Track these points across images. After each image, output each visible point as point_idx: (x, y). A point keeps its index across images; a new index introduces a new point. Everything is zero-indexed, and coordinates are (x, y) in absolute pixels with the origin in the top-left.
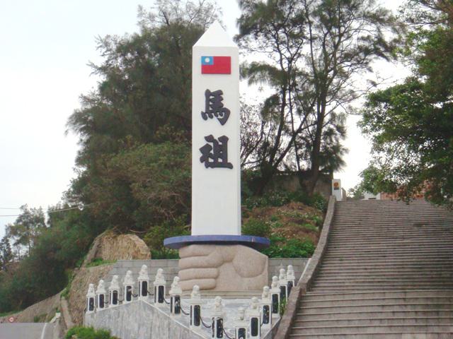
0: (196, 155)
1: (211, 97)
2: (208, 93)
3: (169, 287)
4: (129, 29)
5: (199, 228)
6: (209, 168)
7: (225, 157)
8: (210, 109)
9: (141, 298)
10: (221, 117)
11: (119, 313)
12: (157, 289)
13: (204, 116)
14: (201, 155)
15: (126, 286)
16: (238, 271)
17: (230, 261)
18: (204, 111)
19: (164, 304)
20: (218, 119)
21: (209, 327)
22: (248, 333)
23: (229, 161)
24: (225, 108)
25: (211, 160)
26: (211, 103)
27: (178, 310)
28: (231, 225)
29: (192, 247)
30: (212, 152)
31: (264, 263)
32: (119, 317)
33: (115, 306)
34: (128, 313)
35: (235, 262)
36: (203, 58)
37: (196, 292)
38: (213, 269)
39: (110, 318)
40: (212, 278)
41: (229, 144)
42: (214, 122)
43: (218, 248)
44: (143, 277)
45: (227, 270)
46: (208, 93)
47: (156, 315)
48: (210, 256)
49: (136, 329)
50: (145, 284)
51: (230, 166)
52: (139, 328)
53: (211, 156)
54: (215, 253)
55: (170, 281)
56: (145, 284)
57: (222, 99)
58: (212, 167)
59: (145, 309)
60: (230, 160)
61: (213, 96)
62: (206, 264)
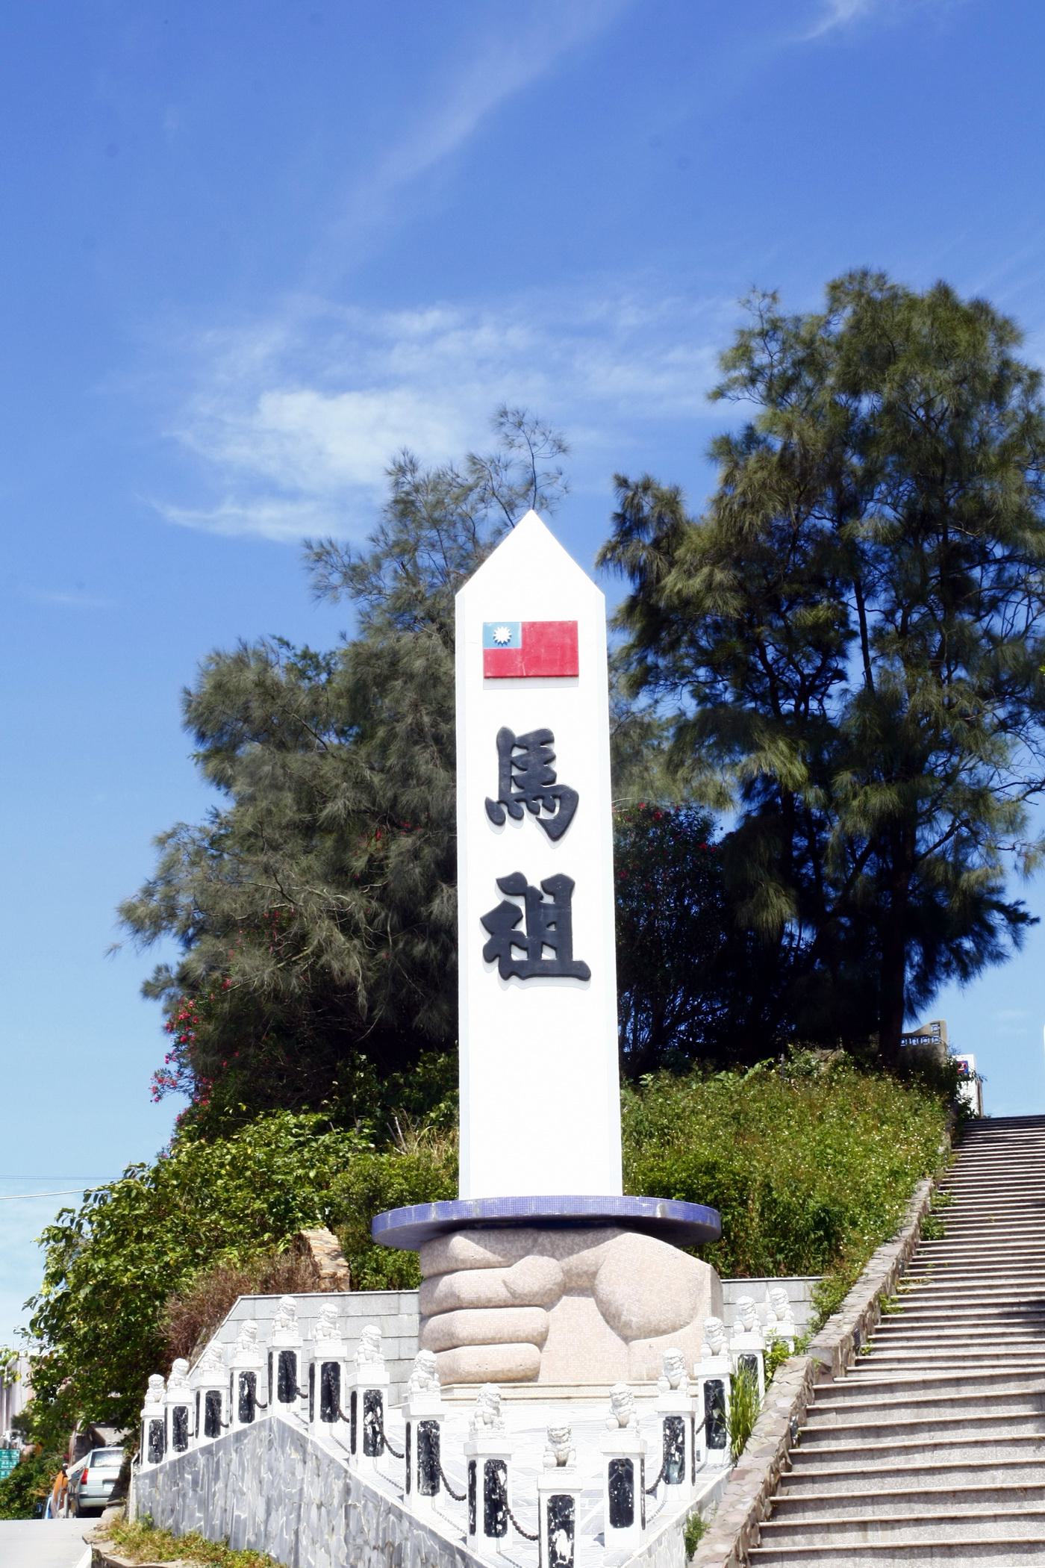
0: (472, 939)
2: (506, 741)
5: (487, 1177)
6: (514, 979)
7: (564, 944)
8: (514, 790)
9: (279, 1410)
11: (218, 1462)
13: (495, 814)
18: (495, 798)
19: (341, 1428)
20: (542, 822)
21: (464, 1498)
22: (592, 1509)
23: (576, 957)
24: (561, 787)
25: (518, 955)
26: (515, 772)
30: (522, 927)
32: (217, 1479)
34: (241, 1463)
36: (488, 630)
46: (506, 741)
51: (582, 973)
52: (268, 1513)
53: (518, 941)
57: (553, 758)
58: (523, 978)
59: (283, 1447)
60: (579, 953)
62: (503, 1294)
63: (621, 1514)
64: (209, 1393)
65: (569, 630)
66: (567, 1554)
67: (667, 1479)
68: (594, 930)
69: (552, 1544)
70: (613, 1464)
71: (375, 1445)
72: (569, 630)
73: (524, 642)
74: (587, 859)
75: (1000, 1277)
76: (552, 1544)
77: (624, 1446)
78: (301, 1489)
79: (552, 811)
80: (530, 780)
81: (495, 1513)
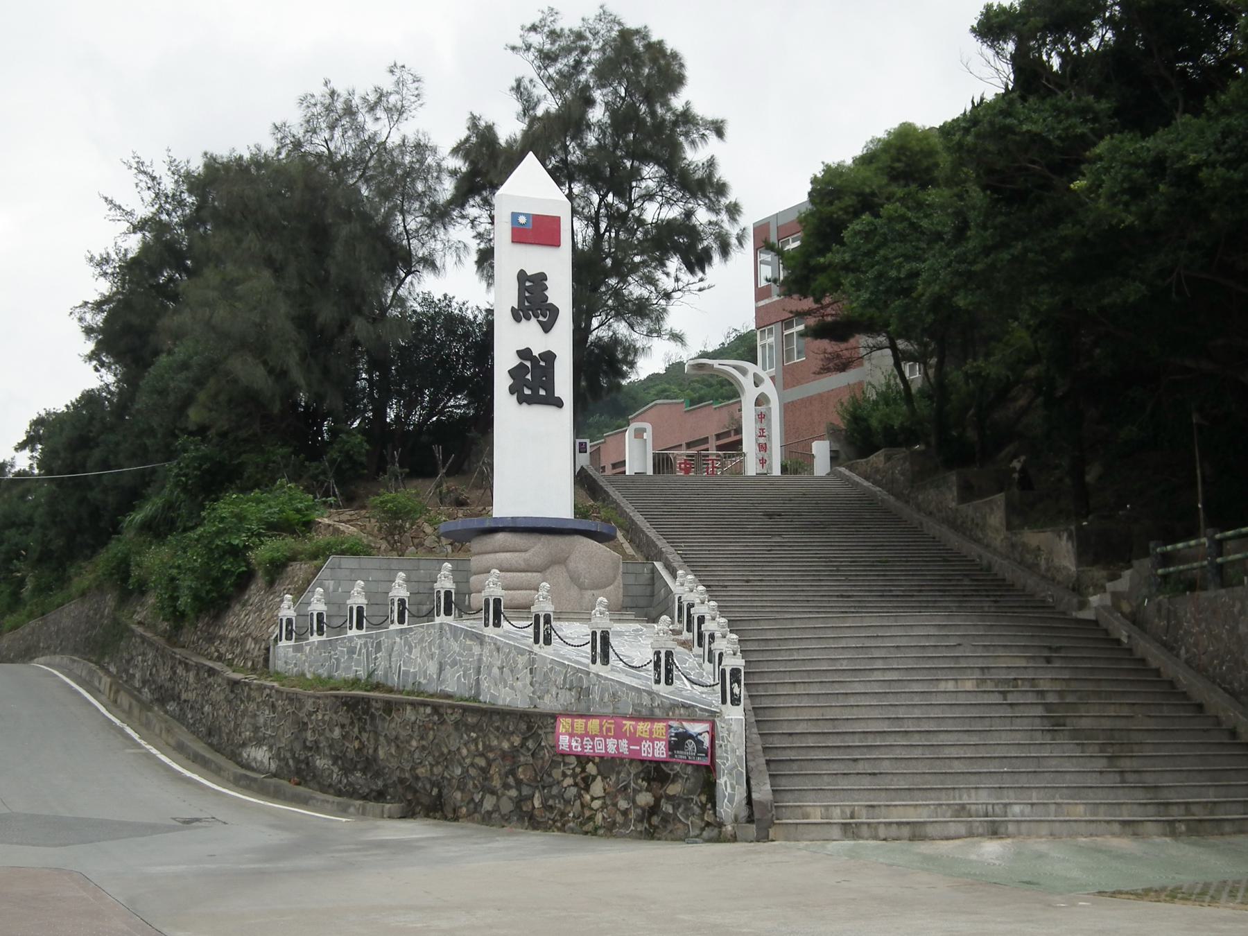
0: (502, 381)
1: (528, 284)
2: (522, 276)
4: (223, 152)
6: (525, 405)
7: (550, 385)
16: (575, 579)
25: (527, 392)
28: (559, 503)
29: (500, 537)
30: (529, 377)
35: (571, 565)
36: (515, 216)
39: (352, 651)
43: (545, 539)
46: (522, 276)
51: (559, 403)
54: (540, 548)
58: (529, 403)
62: (523, 565)
68: (564, 384)
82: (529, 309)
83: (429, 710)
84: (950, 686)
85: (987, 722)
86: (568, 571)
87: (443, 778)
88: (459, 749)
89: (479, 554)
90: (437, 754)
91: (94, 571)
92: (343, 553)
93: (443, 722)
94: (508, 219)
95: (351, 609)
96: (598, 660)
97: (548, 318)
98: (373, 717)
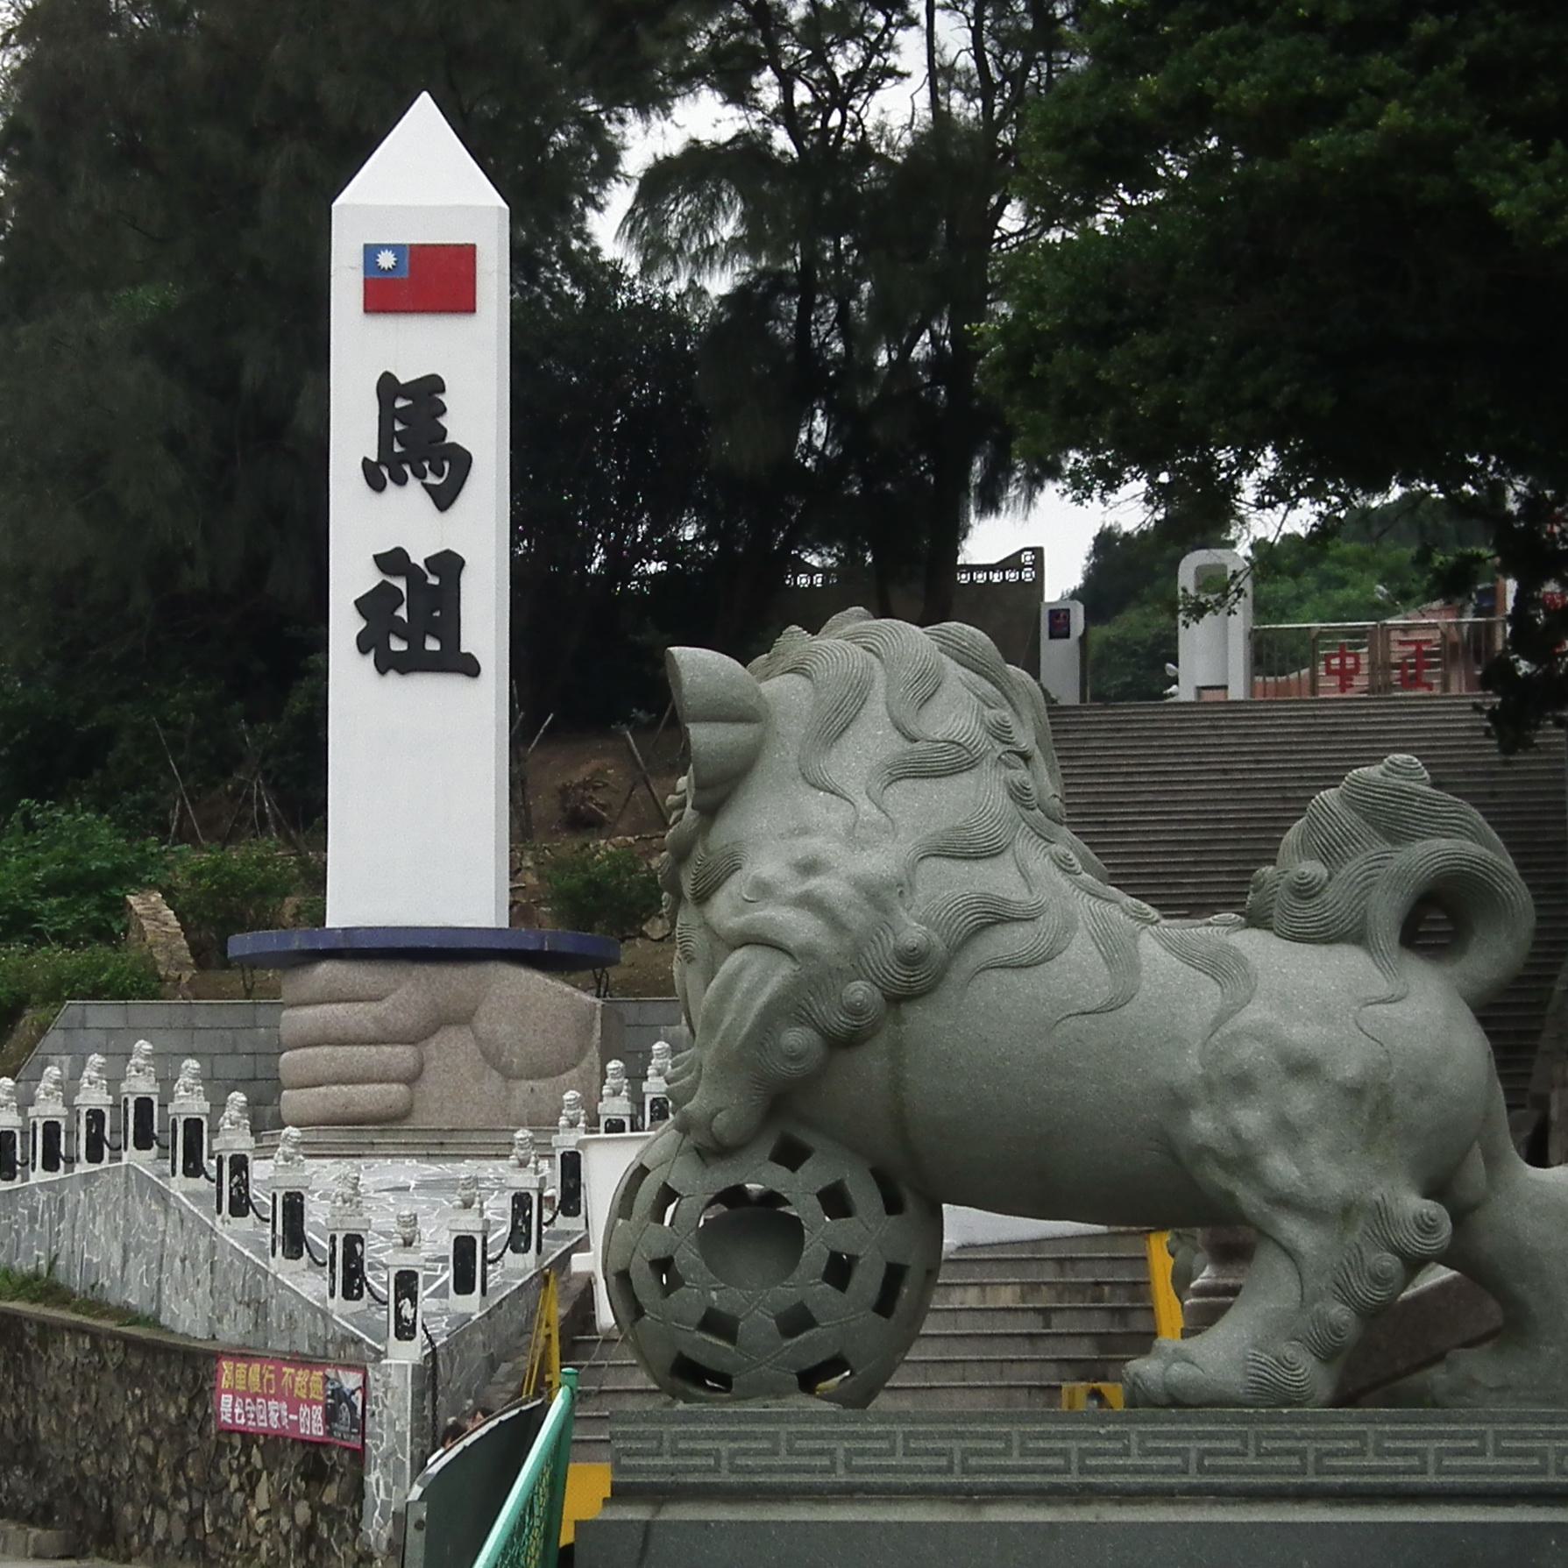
0: (344, 625)
1: (400, 403)
2: (388, 387)
3: (167, 1097)
6: (392, 675)
7: (450, 628)
8: (397, 449)
9: (131, 1155)
10: (438, 481)
11: (62, 1201)
12: (131, 1105)
14: (362, 624)
15: (84, 1111)
16: (492, 1057)
17: (462, 1018)
19: (201, 1184)
20: (425, 486)
23: (463, 650)
24: (454, 446)
25: (397, 645)
26: (398, 427)
27: (240, 1205)
29: (324, 969)
30: (402, 612)
31: (591, 1030)
32: (61, 1218)
33: (51, 1177)
34: (92, 1206)
35: (483, 1026)
36: (371, 252)
37: (235, 1114)
38: (399, 1049)
39: (33, 1218)
40: (397, 1081)
41: (467, 581)
42: (411, 498)
43: (430, 970)
44: (141, 1084)
45: (452, 1054)
46: (388, 387)
47: (175, 1217)
48: (386, 1004)
49: (116, 1261)
50: (144, 1105)
51: (470, 668)
54: (408, 993)
55: (167, 1083)
56: (144, 1105)
59: (142, 1197)
61: (405, 398)
62: (372, 1030)
63: (464, 1283)
64: (46, 1123)
65: (466, 254)
66: (410, 1317)
67: (515, 1250)
68: (485, 620)
69: (398, 1310)
70: (457, 1240)
71: (240, 1205)
72: (466, 254)
73: (412, 270)
74: (477, 531)
75: (1266, 810)
76: (398, 1310)
77: (469, 1223)
78: (163, 1241)
79: (440, 475)
80: (415, 435)
81: (353, 1282)
82: (402, 459)
83: (87, 1343)
84: (971, 1298)
85: (956, 1370)
86: (477, 1039)
87: (111, 1477)
88: (123, 1419)
89: (292, 1006)
90: (102, 1431)
91: (591, 798)
92: (97, 993)
93: (104, 1367)
94: (358, 260)
95: (34, 1124)
96: (279, 1249)
97: (446, 473)
98: (27, 1352)
